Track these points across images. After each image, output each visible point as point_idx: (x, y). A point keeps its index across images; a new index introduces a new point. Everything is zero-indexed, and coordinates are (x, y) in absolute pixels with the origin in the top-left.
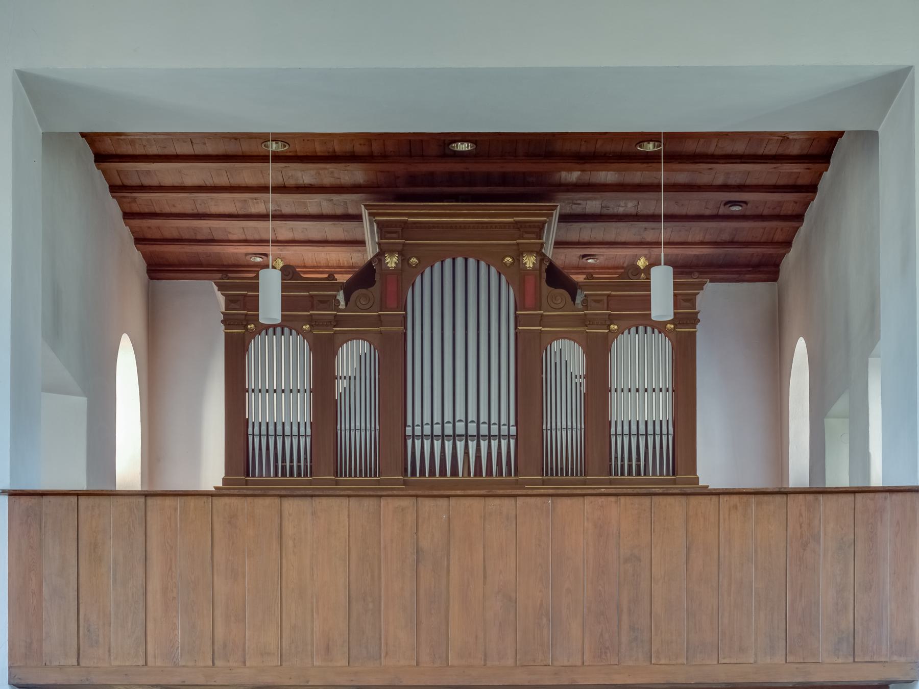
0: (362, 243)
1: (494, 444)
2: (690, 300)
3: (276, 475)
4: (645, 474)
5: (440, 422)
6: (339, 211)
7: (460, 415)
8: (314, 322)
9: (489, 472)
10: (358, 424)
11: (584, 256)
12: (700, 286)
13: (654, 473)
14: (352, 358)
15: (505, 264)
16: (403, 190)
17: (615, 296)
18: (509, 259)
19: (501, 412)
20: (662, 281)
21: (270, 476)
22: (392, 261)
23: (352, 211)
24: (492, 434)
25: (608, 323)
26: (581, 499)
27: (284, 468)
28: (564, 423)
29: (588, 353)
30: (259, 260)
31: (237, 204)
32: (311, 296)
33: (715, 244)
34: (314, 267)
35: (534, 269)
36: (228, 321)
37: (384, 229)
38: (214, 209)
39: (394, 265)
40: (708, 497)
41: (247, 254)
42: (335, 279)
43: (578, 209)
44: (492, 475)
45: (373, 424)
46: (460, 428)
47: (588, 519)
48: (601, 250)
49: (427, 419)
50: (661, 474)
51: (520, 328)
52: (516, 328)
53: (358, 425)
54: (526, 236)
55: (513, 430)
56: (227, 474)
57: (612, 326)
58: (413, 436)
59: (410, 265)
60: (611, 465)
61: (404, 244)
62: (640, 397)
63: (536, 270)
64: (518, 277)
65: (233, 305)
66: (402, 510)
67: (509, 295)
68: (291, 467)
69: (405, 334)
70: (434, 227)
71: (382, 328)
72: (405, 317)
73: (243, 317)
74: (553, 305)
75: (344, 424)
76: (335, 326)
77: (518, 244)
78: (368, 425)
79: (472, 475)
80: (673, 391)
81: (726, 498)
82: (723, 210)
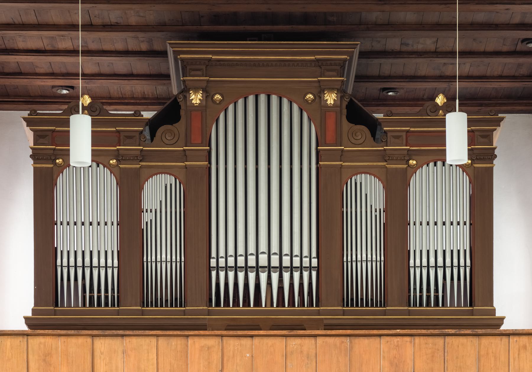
0: (167, 77)
1: (296, 275)
2: (488, 137)
3: (84, 305)
4: (443, 306)
5: (244, 254)
6: (144, 47)
7: (263, 247)
8: (120, 157)
9: (292, 303)
10: (164, 256)
11: (384, 89)
12: (498, 122)
13: (452, 304)
14: (158, 192)
15: (307, 101)
16: (206, 28)
17: (413, 132)
18: (310, 96)
19: (301, 244)
20: (456, 127)
21: (78, 306)
22: (196, 98)
23: (157, 47)
24: (294, 265)
25: (407, 158)
26: (377, 339)
27: (91, 298)
28: (364, 255)
29: (387, 188)
30: (65, 92)
31: (44, 40)
32: (118, 132)
33: (513, 78)
34: (119, 98)
35: (335, 105)
36: (36, 156)
37: (186, 67)
38: (21, 45)
39: (198, 102)
40: (499, 338)
41: (53, 87)
42: (142, 116)
43: (378, 47)
44: (294, 306)
45: (178, 257)
46: (263, 260)
47: (384, 357)
48: (402, 84)
49: (231, 251)
50: (459, 305)
51: (321, 163)
52: (317, 163)
53: (164, 255)
54: (327, 73)
55: (315, 262)
56: (36, 304)
57: (411, 162)
58: (218, 268)
59: (214, 102)
60: (410, 296)
61: (208, 81)
62: (437, 233)
63: (337, 107)
64: (318, 113)
65: (41, 141)
66: (209, 348)
67: (311, 132)
68: (99, 298)
69: (210, 169)
70: (237, 65)
71: (187, 163)
72: (210, 152)
73: (52, 152)
74: (353, 141)
75: (150, 257)
76: (141, 161)
77: (319, 81)
78: (174, 257)
79: (275, 305)
80: (471, 224)
81: (516, 338)
82: (521, 47)
